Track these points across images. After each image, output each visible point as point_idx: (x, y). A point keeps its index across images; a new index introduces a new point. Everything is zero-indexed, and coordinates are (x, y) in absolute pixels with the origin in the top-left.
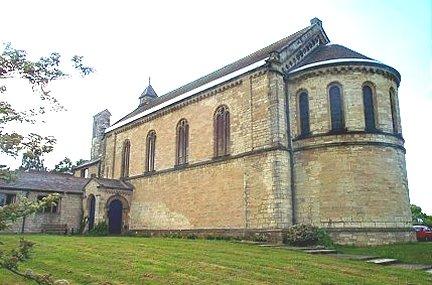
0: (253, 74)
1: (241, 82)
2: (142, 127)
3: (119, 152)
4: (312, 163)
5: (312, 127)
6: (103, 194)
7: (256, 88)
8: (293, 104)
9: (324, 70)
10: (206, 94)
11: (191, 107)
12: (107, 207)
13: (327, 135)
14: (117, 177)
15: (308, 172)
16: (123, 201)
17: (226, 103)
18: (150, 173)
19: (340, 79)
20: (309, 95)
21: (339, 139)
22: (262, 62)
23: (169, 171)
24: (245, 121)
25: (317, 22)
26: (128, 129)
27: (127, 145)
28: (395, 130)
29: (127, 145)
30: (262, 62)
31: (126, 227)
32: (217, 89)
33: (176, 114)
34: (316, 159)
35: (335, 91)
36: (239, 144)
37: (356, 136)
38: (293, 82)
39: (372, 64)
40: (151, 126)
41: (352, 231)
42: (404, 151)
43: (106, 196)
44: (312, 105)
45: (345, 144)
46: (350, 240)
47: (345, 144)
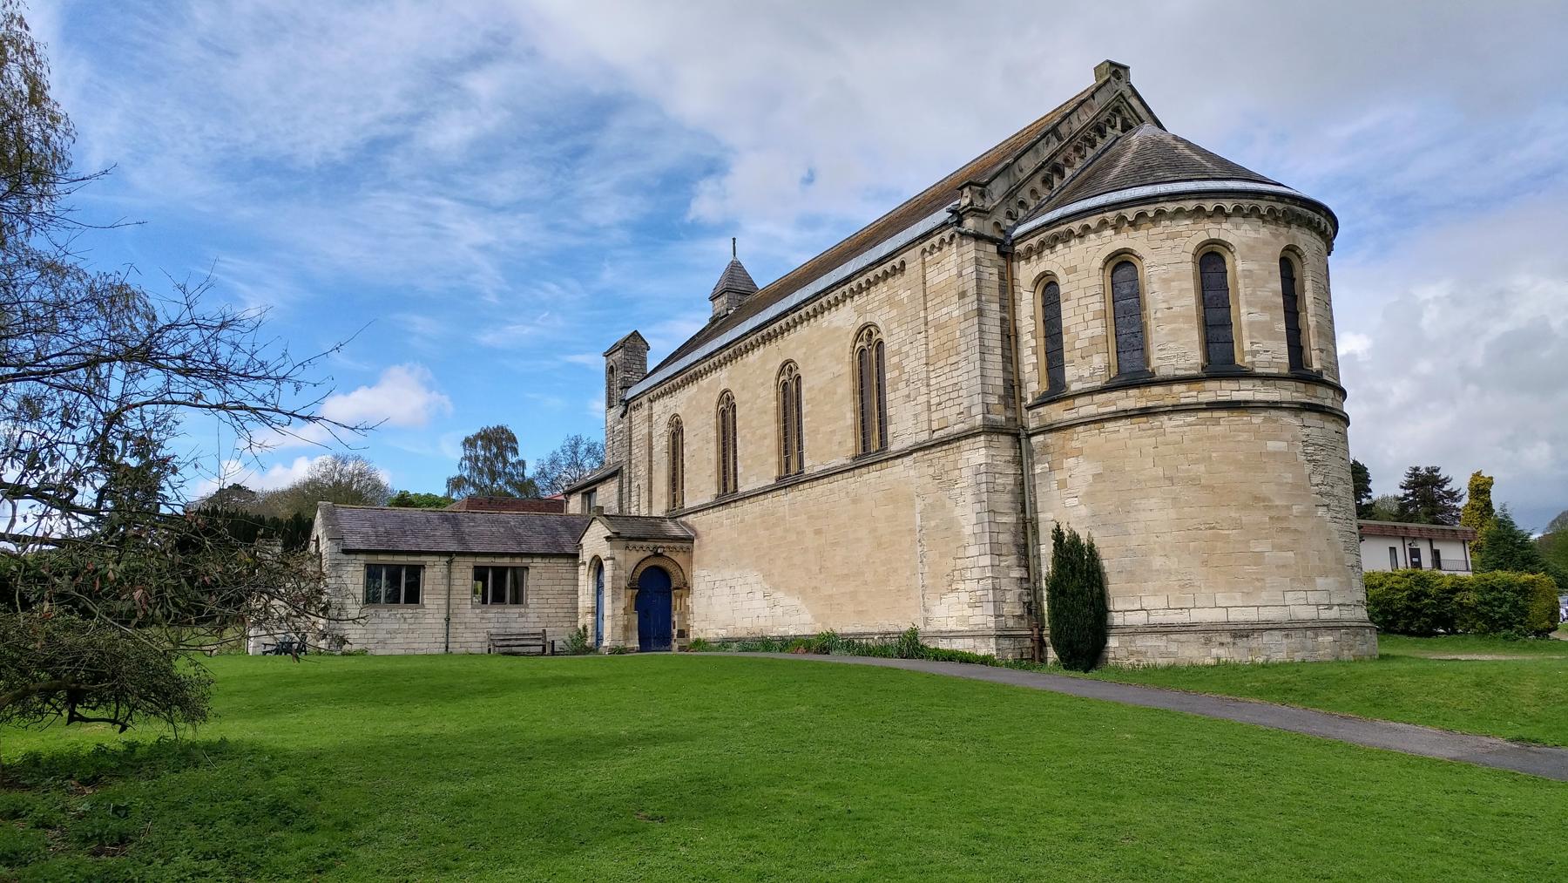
0: (927, 244)
1: (903, 263)
2: (704, 382)
3: (661, 444)
4: (1071, 462)
5: (1070, 373)
6: (619, 556)
7: (935, 277)
8: (1028, 309)
9: (1093, 221)
10: (831, 297)
11: (803, 330)
12: (631, 586)
13: (1103, 390)
14: (659, 509)
15: (1062, 484)
16: (671, 568)
17: (876, 320)
18: (728, 494)
19: (1228, 232)
20: (1063, 290)
21: (1131, 399)
22: (942, 215)
23: (765, 492)
24: (913, 365)
25: (1117, 71)
26: (675, 389)
27: (677, 430)
28: (1299, 371)
29: (677, 430)
30: (942, 215)
31: (682, 634)
32: (854, 284)
33: (772, 347)
34: (1079, 453)
35: (1211, 260)
36: (904, 426)
37: (1177, 388)
38: (1028, 255)
39: (1280, 197)
40: (722, 379)
41: (1165, 630)
42: (1345, 420)
43: (632, 558)
44: (1069, 316)
45: (1146, 412)
46: (1162, 655)
47: (1146, 412)
